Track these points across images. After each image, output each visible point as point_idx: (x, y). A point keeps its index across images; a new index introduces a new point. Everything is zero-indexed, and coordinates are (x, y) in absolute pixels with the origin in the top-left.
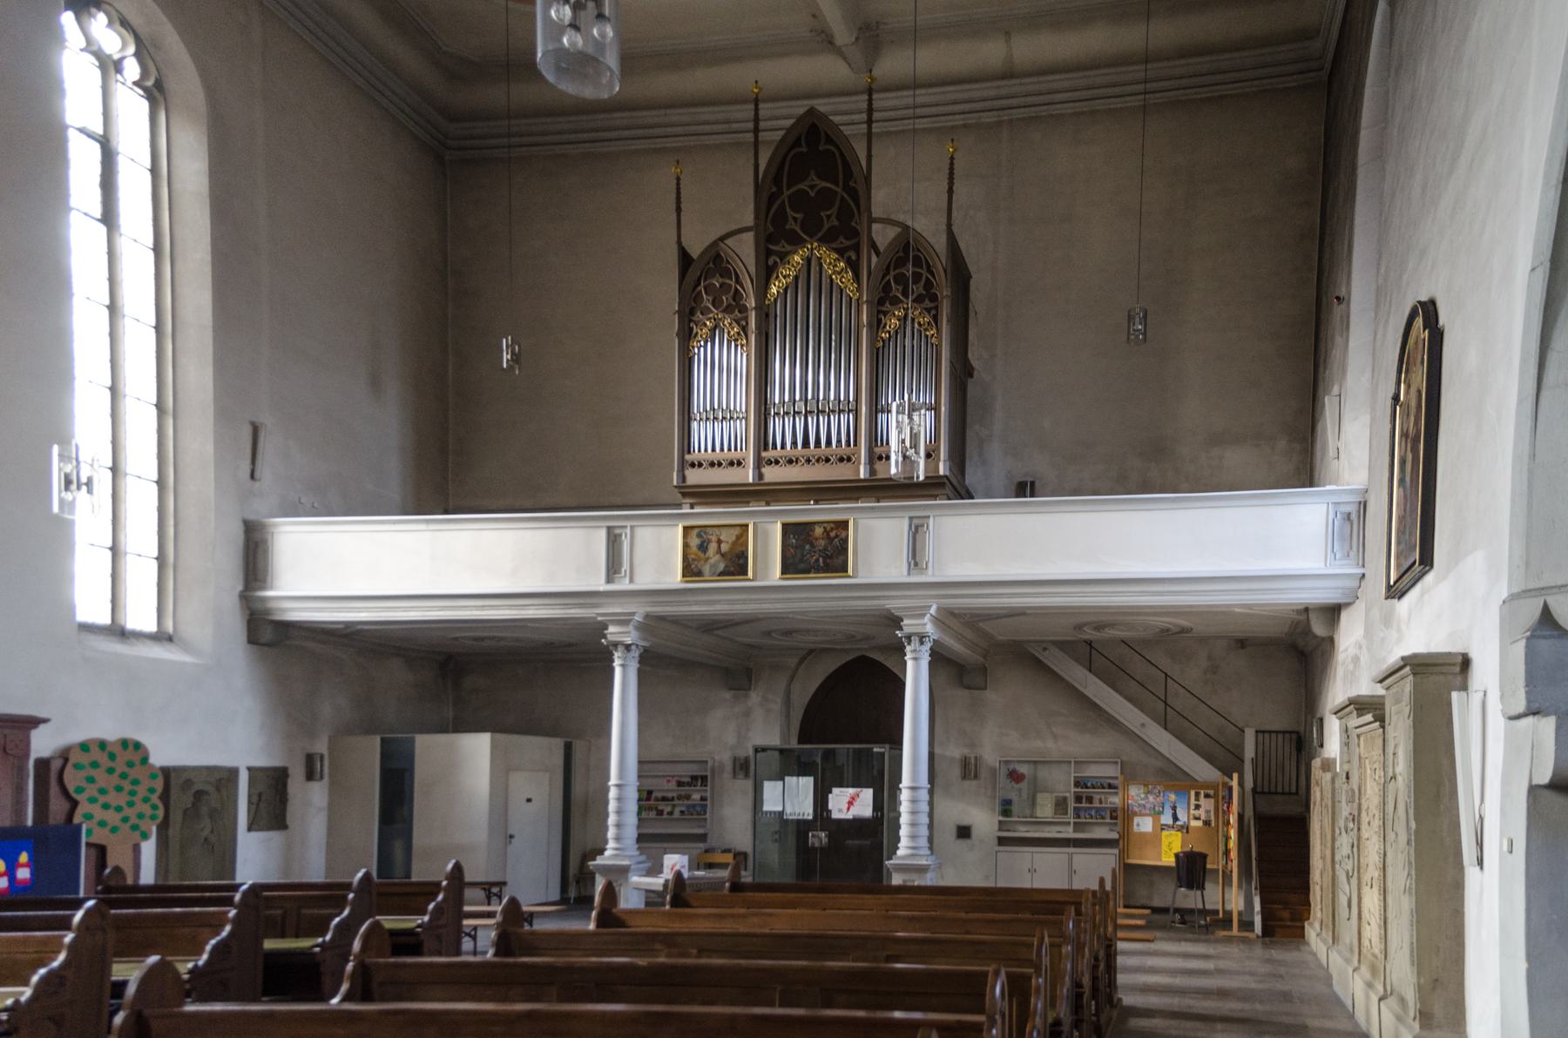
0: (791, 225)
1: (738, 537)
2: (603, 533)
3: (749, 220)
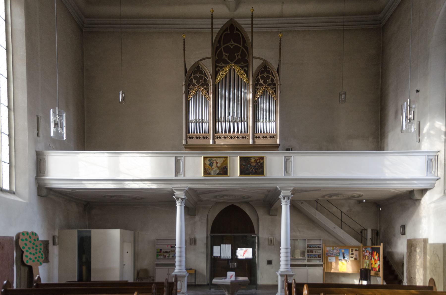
0: (224, 57)
1: (224, 162)
2: (174, 159)
3: (210, 55)
